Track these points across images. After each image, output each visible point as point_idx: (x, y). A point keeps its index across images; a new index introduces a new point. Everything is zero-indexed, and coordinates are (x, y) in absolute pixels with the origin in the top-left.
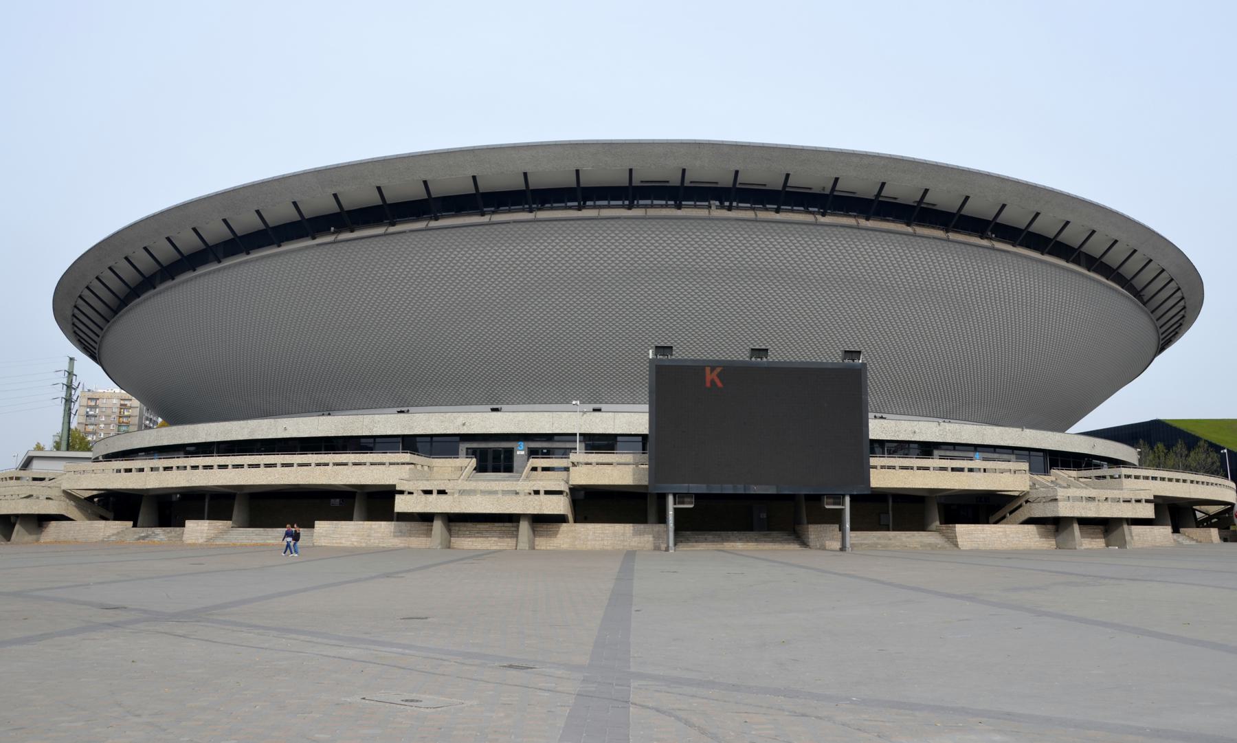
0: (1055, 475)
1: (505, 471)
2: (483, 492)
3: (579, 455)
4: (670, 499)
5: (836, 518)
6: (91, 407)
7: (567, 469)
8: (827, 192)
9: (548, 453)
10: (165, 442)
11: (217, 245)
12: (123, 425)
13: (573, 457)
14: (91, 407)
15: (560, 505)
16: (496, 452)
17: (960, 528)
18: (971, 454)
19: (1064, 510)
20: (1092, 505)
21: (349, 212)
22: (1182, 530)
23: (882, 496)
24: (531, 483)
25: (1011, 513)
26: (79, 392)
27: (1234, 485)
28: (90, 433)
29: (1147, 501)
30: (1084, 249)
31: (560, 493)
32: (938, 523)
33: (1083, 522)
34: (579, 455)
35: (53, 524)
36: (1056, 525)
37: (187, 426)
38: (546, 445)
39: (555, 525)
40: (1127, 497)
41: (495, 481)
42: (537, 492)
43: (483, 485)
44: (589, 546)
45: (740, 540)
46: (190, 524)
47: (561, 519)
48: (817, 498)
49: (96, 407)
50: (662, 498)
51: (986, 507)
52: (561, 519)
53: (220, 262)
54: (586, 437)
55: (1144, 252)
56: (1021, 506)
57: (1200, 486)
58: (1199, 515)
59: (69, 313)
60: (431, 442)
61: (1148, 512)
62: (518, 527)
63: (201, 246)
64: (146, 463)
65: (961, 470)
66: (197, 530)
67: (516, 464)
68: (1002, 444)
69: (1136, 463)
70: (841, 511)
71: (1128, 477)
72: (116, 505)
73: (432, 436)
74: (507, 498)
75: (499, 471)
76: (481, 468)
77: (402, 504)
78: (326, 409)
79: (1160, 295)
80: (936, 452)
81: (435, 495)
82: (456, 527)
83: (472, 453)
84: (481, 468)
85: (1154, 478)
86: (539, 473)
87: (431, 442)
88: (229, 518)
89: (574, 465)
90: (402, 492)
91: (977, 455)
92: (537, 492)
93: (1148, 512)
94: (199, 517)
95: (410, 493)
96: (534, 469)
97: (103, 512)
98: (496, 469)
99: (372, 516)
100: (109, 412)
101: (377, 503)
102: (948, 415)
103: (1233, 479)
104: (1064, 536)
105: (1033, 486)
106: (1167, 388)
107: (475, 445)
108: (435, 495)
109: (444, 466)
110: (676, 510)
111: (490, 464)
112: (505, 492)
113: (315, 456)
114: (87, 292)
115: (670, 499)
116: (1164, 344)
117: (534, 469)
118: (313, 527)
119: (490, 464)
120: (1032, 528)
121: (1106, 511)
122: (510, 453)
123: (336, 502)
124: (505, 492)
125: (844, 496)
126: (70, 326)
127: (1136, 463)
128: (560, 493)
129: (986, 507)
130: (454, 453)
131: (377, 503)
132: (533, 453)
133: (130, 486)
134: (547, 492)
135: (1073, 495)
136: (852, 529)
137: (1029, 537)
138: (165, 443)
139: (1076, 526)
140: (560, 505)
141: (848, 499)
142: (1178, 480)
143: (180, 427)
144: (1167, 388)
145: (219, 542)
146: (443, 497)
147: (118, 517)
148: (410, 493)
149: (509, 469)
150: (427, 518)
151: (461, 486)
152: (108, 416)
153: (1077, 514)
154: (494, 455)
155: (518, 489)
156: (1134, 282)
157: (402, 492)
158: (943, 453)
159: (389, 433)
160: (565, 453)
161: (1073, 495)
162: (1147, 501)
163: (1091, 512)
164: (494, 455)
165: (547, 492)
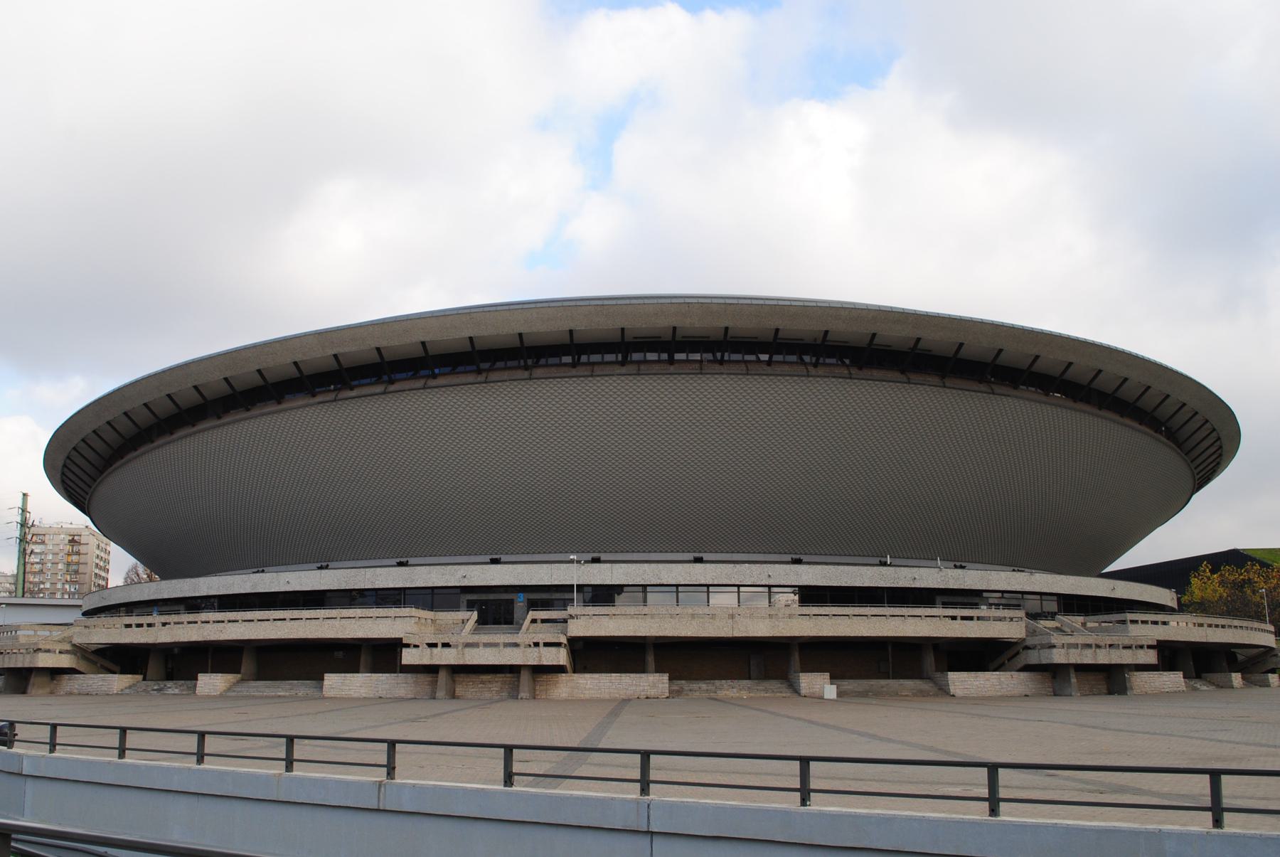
0: (1060, 621)
1: (506, 623)
2: (486, 645)
7: (565, 621)
8: (819, 342)
12: (130, 582)
13: (571, 610)
15: (560, 657)
17: (953, 676)
19: (1058, 657)
20: (1089, 652)
21: (242, 393)
24: (530, 636)
26: (33, 530)
27: (1272, 628)
29: (1149, 647)
31: (558, 645)
33: (1081, 668)
35: (66, 677)
38: (548, 597)
39: (554, 676)
40: (1127, 642)
41: (500, 635)
42: (536, 644)
43: (484, 638)
44: (587, 695)
47: (560, 669)
53: (219, 418)
54: (581, 588)
56: (1018, 653)
57: (1239, 631)
58: (1240, 658)
59: (61, 464)
60: (433, 594)
61: (1151, 657)
62: (519, 678)
64: (157, 619)
65: (971, 618)
66: (211, 683)
68: (1009, 589)
69: (1175, 605)
71: (1133, 622)
73: (433, 588)
74: (509, 650)
75: (500, 623)
77: (408, 657)
78: (259, 566)
79: (1184, 430)
80: (939, 599)
81: (145, 627)
82: (460, 678)
83: (471, 606)
84: (482, 621)
85: (1155, 623)
86: (539, 625)
87: (433, 594)
88: (235, 670)
89: (571, 617)
90: (408, 646)
92: (536, 644)
93: (1151, 657)
95: (416, 646)
96: (534, 621)
98: (497, 622)
101: (384, 655)
103: (1271, 622)
105: (1032, 632)
106: (1204, 525)
107: (484, 597)
108: (145, 627)
112: (506, 645)
113: (323, 611)
114: (83, 444)
116: (1202, 480)
117: (534, 621)
120: (1023, 675)
121: (1103, 658)
122: (511, 602)
123: (339, 654)
124: (506, 645)
126: (59, 476)
127: (1175, 605)
128: (558, 645)
130: (454, 607)
131: (384, 655)
132: (533, 605)
133: (143, 641)
134: (546, 645)
135: (1073, 642)
140: (65, 661)
142: (1217, 626)
143: (181, 581)
144: (1204, 525)
146: (447, 650)
148: (416, 646)
149: (509, 621)
150: (432, 670)
153: (1072, 661)
154: (495, 608)
155: (518, 641)
157: (408, 646)
158: (946, 599)
159: (391, 586)
160: (565, 604)
161: (1073, 642)
162: (1149, 647)
163: (1088, 658)
164: (495, 608)
165: (546, 645)
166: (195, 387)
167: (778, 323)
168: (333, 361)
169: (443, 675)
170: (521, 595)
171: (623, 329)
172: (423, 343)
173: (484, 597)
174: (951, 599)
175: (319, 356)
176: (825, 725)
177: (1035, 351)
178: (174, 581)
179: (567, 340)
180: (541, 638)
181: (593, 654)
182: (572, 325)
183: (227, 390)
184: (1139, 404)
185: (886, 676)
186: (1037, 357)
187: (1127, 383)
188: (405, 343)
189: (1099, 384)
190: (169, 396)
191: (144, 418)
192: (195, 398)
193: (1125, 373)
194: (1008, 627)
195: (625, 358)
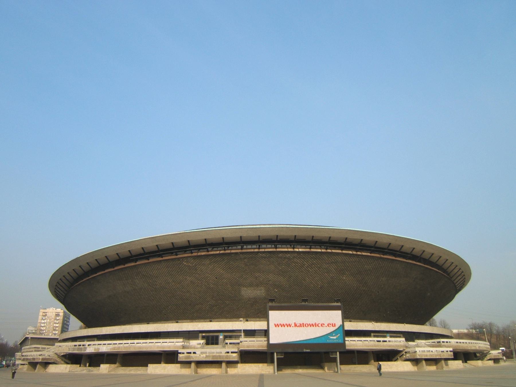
3: (243, 339)
4: (275, 354)
5: (334, 360)
6: (44, 316)
7: (239, 343)
9: (230, 337)
10: (90, 334)
11: (113, 261)
14: (44, 316)
15: (235, 357)
16: (213, 337)
18: (385, 334)
21: (122, 259)
22: (468, 362)
23: (352, 352)
25: (400, 357)
27: (489, 344)
28: (42, 327)
30: (422, 256)
32: (373, 361)
34: (243, 339)
35: (51, 365)
36: (416, 361)
37: (98, 328)
38: (231, 334)
39: (235, 365)
45: (301, 368)
46: (102, 365)
48: (327, 353)
49: (46, 315)
50: (272, 354)
51: (391, 355)
52: (236, 362)
55: (444, 257)
63: (107, 261)
67: (220, 341)
68: (397, 330)
70: (336, 358)
72: (73, 359)
76: (207, 343)
78: (148, 321)
83: (203, 338)
89: (241, 342)
90: (180, 353)
91: (388, 335)
94: (103, 363)
97: (67, 361)
98: (212, 344)
99: (168, 362)
100: (51, 318)
101: (171, 357)
102: (377, 320)
104: (420, 365)
107: (208, 334)
109: (193, 343)
110: (277, 359)
111: (210, 342)
114: (64, 278)
115: (275, 354)
118: (100, 366)
119: (210, 342)
120: (409, 363)
122: (217, 337)
125: (336, 352)
129: (391, 355)
131: (171, 357)
132: (226, 337)
136: (341, 364)
137: (406, 367)
138: (90, 334)
139: (424, 362)
140: (235, 357)
141: (338, 353)
145: (112, 373)
147: (73, 363)
149: (217, 343)
150: (189, 363)
151: (198, 349)
152: (50, 320)
154: (211, 338)
156: (443, 267)
157: (180, 353)
158: (375, 334)
160: (238, 337)
164: (211, 338)
166: (106, 257)
167: (296, 234)
168: (156, 247)
169: (193, 365)
170: (222, 334)
171: (277, 236)
172: (189, 241)
173: (208, 334)
174: (377, 334)
175: (324, 235)
176: (334, 381)
177: (402, 244)
178: (94, 329)
179: (204, 243)
180: (230, 350)
181: (248, 356)
182: (223, 236)
183: (117, 258)
184: (437, 263)
185: (354, 364)
186: (403, 246)
187: (433, 256)
188: (181, 241)
189: (424, 256)
190: (96, 260)
191: (86, 268)
192: (106, 261)
193: (432, 251)
194: (398, 343)
195: (259, 246)
